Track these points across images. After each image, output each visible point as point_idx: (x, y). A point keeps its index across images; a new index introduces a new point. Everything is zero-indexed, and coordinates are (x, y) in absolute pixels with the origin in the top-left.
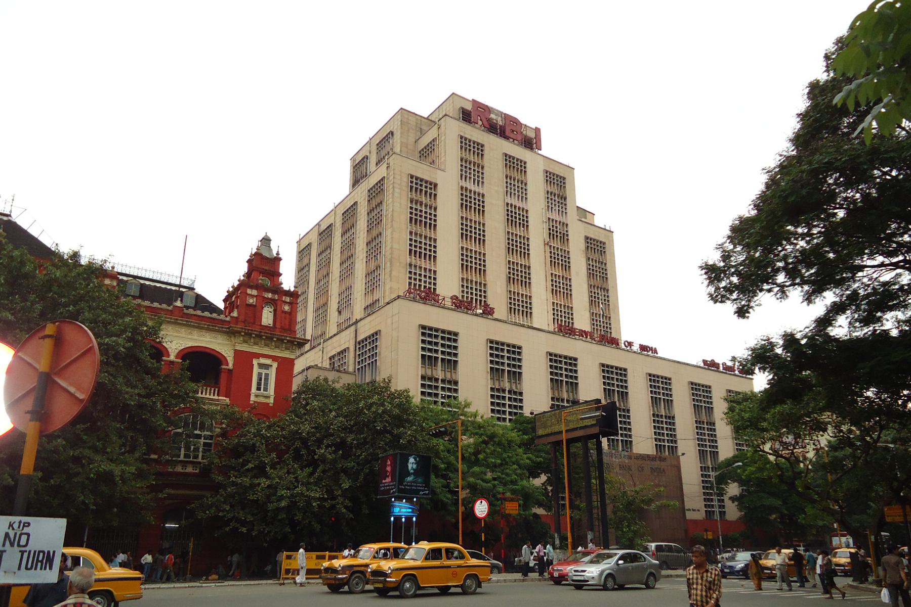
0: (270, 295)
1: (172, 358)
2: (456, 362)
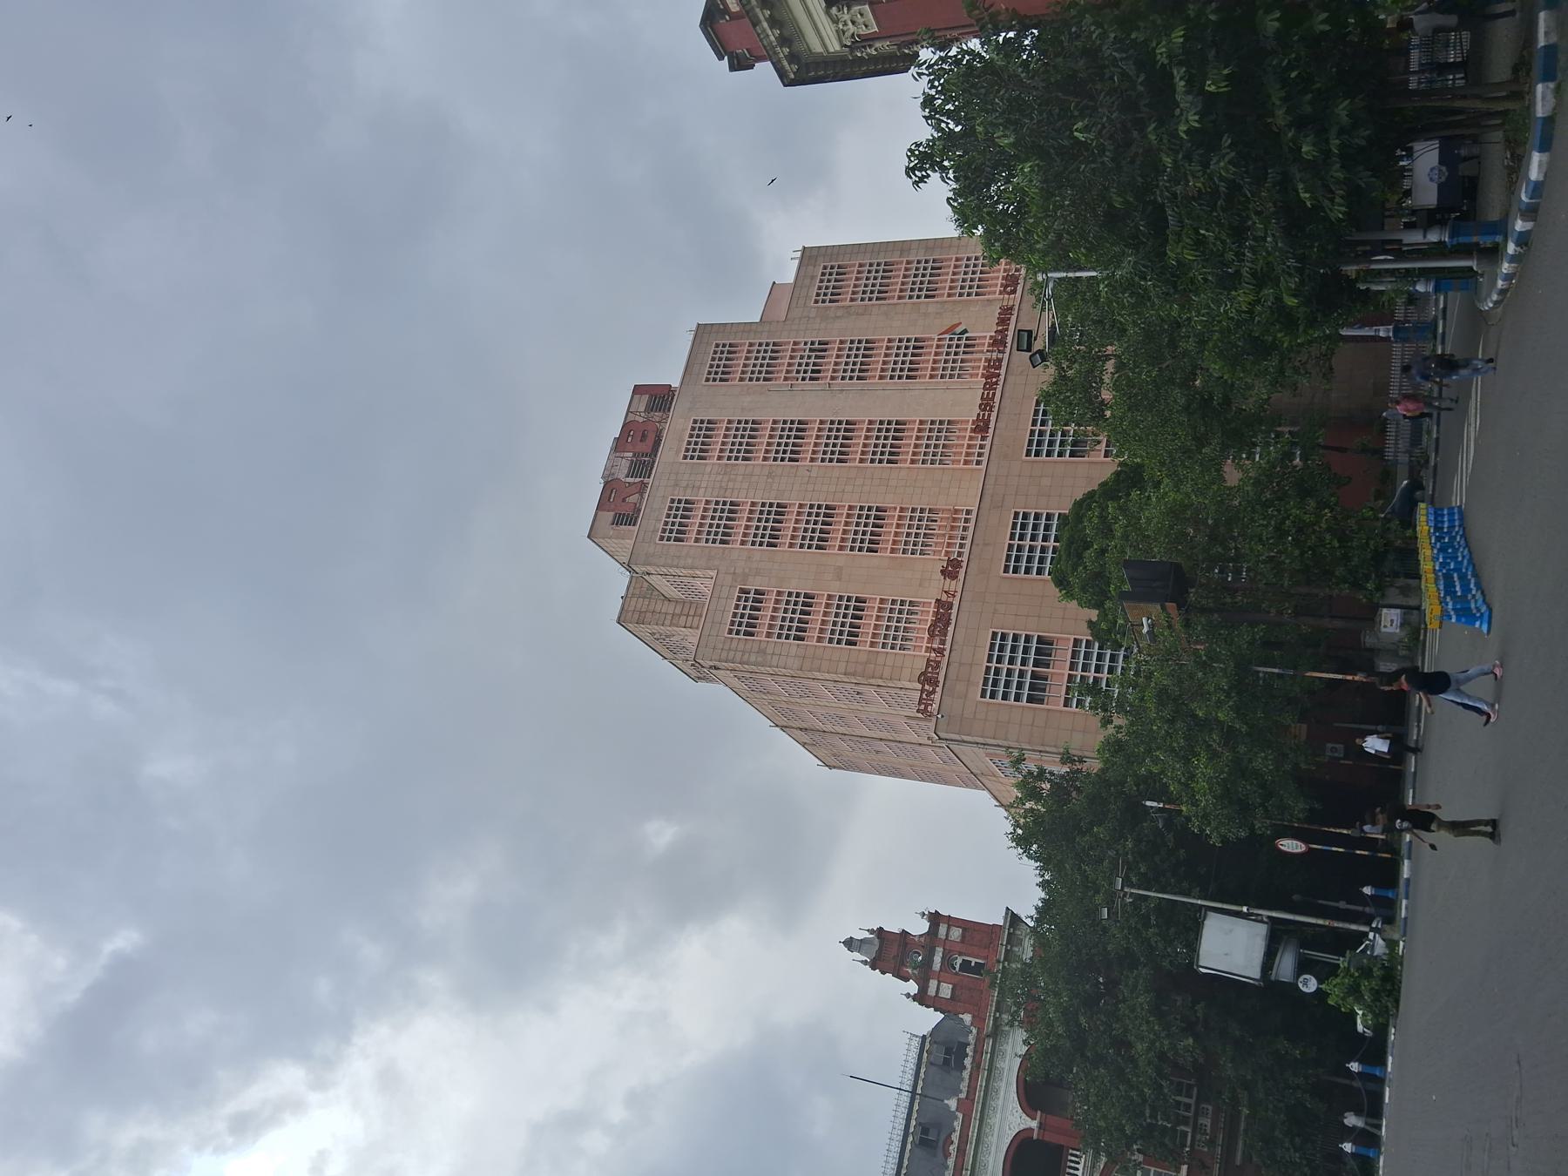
0: (938, 959)
1: (1034, 1124)
2: (1040, 640)
